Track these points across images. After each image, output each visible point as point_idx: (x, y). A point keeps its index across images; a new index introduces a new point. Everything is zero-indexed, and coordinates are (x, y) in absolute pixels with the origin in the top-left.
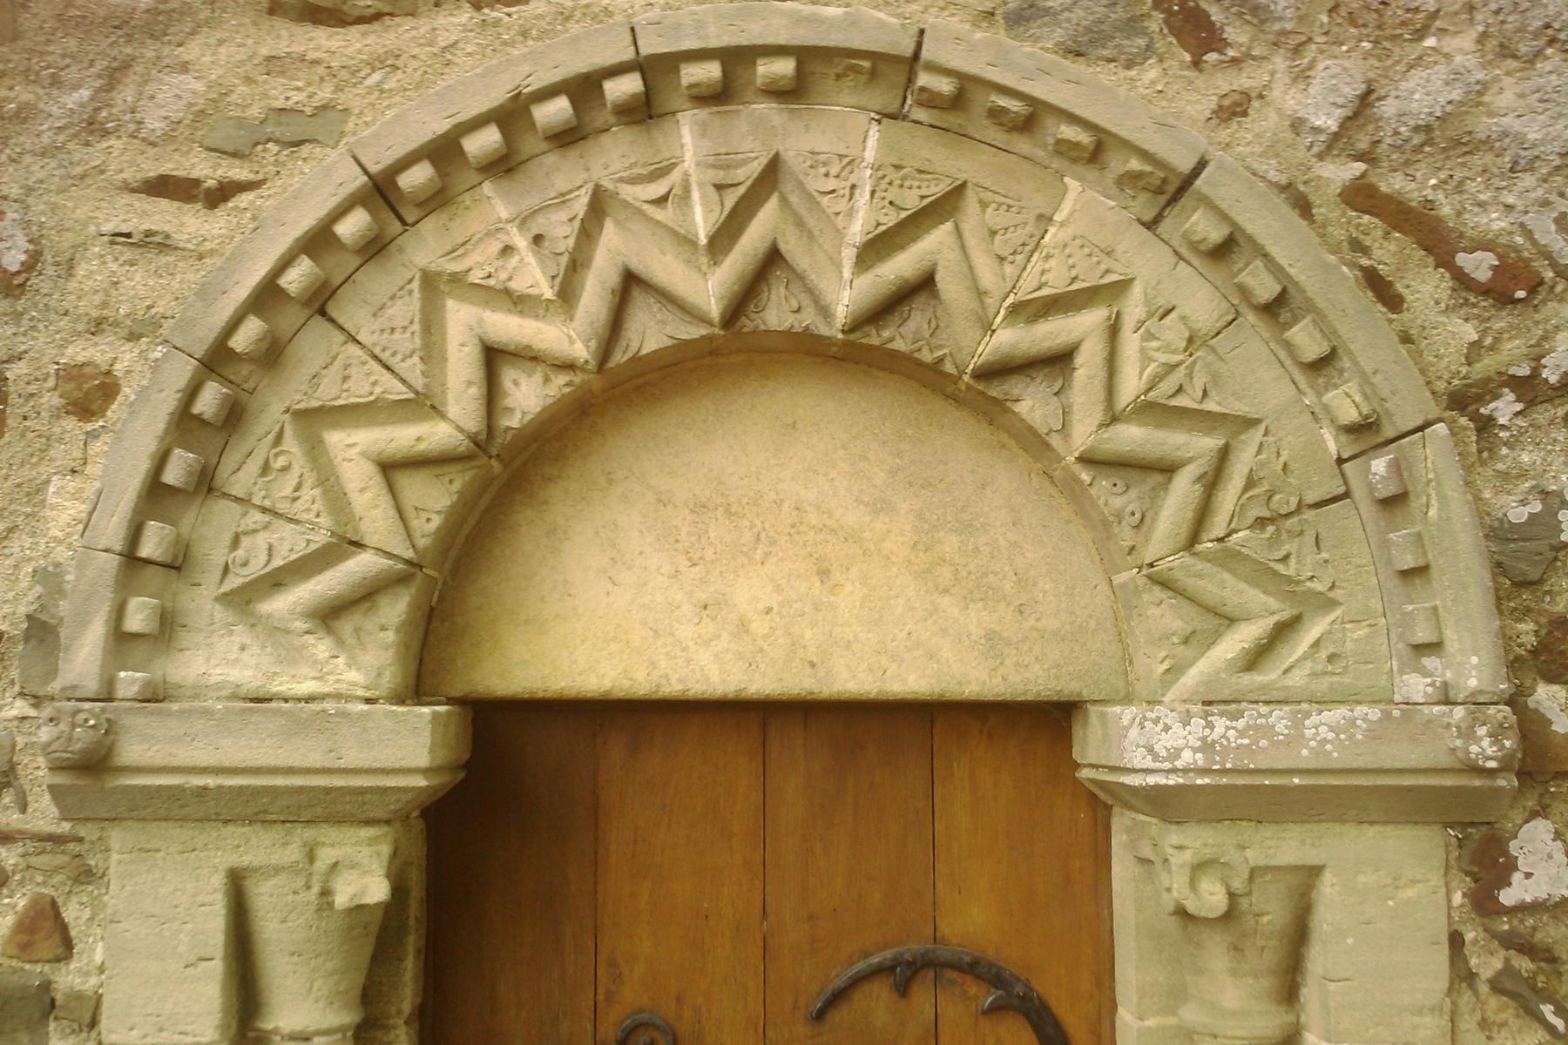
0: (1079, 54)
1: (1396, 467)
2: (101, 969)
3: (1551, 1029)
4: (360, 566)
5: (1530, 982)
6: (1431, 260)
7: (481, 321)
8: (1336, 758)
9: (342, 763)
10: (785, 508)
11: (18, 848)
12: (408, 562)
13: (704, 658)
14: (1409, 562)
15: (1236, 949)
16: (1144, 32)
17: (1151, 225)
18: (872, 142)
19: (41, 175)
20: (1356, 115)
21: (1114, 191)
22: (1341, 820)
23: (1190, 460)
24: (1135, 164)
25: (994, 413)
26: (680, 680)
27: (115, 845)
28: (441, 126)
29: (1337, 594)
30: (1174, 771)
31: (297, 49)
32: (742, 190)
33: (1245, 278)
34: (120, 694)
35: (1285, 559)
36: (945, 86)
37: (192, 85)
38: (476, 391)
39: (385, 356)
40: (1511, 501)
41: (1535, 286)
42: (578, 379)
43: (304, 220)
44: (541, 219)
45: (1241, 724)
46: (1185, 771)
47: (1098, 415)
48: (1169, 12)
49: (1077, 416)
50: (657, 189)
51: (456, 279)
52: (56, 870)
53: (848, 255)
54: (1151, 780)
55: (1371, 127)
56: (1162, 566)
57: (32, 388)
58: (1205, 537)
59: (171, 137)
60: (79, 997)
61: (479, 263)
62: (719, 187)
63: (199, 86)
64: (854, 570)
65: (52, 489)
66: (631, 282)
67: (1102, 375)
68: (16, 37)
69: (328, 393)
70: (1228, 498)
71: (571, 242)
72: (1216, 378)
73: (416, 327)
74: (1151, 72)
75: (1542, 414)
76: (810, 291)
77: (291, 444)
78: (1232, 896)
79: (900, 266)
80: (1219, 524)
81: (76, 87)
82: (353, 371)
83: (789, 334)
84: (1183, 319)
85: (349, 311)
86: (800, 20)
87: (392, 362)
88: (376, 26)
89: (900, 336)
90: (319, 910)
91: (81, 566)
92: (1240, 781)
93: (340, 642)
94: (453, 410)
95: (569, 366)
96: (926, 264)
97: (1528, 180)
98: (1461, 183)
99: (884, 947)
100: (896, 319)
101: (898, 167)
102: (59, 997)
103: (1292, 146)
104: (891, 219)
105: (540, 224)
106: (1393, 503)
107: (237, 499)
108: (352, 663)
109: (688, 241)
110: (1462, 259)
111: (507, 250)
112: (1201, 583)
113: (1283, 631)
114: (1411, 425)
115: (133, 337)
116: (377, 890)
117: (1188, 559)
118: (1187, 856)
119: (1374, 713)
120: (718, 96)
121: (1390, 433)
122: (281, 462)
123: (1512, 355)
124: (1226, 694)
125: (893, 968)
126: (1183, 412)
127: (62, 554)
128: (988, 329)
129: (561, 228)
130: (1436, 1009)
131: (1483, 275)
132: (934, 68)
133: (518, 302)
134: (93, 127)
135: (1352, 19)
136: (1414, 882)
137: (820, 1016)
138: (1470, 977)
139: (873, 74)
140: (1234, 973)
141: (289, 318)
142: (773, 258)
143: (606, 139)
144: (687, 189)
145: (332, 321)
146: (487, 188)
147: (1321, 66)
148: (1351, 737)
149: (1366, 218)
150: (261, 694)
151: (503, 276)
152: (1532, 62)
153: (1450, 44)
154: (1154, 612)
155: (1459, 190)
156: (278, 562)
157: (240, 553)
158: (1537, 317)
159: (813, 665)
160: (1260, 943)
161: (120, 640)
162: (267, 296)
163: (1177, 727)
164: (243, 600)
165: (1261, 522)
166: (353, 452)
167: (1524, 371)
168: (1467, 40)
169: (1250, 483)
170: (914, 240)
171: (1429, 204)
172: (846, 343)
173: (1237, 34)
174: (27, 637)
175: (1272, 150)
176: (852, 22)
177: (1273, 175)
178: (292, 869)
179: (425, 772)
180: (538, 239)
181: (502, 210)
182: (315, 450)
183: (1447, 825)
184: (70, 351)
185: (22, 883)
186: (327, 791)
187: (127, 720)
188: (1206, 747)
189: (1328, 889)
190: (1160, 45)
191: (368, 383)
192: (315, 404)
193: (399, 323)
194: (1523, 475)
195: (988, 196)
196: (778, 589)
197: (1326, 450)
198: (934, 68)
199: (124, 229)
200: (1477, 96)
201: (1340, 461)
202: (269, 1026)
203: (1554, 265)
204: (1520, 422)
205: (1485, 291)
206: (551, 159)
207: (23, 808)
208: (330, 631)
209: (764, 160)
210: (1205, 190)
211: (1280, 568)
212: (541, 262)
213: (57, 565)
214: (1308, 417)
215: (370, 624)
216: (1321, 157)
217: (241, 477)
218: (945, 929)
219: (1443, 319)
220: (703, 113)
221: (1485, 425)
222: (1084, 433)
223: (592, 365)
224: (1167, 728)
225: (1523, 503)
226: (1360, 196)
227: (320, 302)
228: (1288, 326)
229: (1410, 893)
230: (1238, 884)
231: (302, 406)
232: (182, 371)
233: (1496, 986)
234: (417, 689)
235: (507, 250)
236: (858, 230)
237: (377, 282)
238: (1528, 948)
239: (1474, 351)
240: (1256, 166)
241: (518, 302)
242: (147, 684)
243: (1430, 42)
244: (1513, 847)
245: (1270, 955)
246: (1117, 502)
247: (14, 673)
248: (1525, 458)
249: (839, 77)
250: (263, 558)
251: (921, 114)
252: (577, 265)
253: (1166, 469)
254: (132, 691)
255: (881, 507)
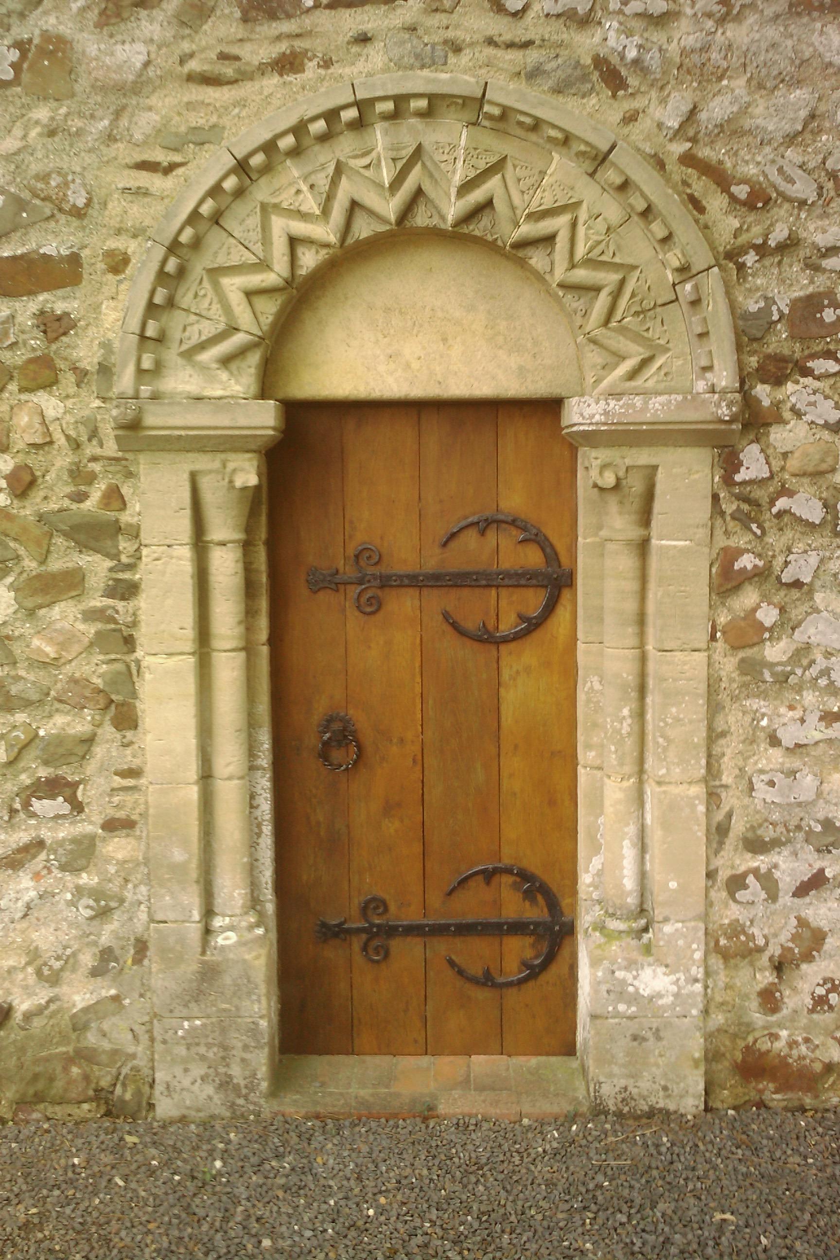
0: (559, 92)
1: (696, 288)
2: (139, 514)
3: (755, 534)
4: (239, 339)
5: (748, 515)
6: (719, 190)
7: (288, 226)
8: (662, 417)
9: (238, 425)
10: (427, 310)
11: (101, 463)
12: (259, 337)
13: (390, 380)
14: (699, 330)
15: (621, 503)
16: (590, 81)
17: (592, 175)
18: (464, 137)
19: (89, 161)
20: (688, 119)
21: (575, 158)
22: (666, 445)
23: (606, 285)
24: (583, 148)
25: (522, 263)
26: (380, 391)
27: (142, 461)
28: (267, 136)
29: (670, 345)
30: (591, 424)
31: (200, 98)
32: (404, 161)
33: (632, 200)
34: (142, 395)
35: (648, 329)
36: (496, 111)
37: (155, 117)
38: (286, 259)
39: (246, 243)
40: (752, 302)
41: (767, 201)
42: (331, 252)
43: (209, 182)
44: (313, 177)
45: (621, 403)
46: (597, 424)
47: (566, 265)
48: (601, 71)
49: (556, 265)
50: (365, 161)
51: (276, 206)
52: (118, 472)
53: (453, 191)
54: (582, 428)
55: (695, 125)
56: (593, 334)
57: (93, 261)
58: (613, 320)
59: (144, 144)
60: (131, 525)
61: (286, 199)
62: (394, 160)
63: (157, 118)
64: (458, 339)
65: (104, 306)
66: (354, 205)
67: (568, 246)
68: (73, 95)
69: (222, 260)
70: (623, 303)
71: (327, 187)
72: (619, 247)
73: (259, 229)
74: (593, 100)
75: (767, 262)
76: (436, 207)
77: (206, 284)
78: (618, 479)
79: (477, 196)
80: (618, 315)
81: (101, 119)
82: (232, 250)
83: (427, 228)
84: (605, 219)
85: (229, 222)
86: (428, 81)
87: (249, 246)
88: (235, 86)
89: (476, 229)
90: (229, 489)
91: (122, 340)
92: (620, 428)
93: (231, 373)
94: (277, 267)
95: (327, 245)
96: (489, 195)
97: (767, 149)
98: (737, 151)
99: (474, 514)
100: (476, 220)
101: (476, 149)
102: (123, 526)
103: (657, 135)
104: (472, 174)
105: (313, 179)
106: (695, 303)
107: (184, 310)
108: (237, 382)
109: (381, 186)
110: (734, 189)
111: (298, 192)
112: (609, 342)
113: (645, 363)
114: (702, 268)
115: (135, 236)
116: (253, 480)
117: (603, 330)
118: (599, 461)
119: (680, 398)
120: (394, 116)
121: (694, 271)
122: (202, 293)
123: (755, 235)
124: (618, 391)
125: (478, 523)
126: (604, 263)
127: (111, 335)
128: (517, 225)
129: (323, 181)
130: (704, 526)
131: (743, 196)
132: (491, 103)
133: (304, 216)
134: (110, 138)
135: (689, 72)
136: (697, 472)
137: (445, 545)
138: (722, 513)
139: (464, 105)
140: (620, 513)
141: (203, 226)
142: (419, 193)
143: (341, 138)
144: (379, 161)
145: (221, 227)
146: (288, 162)
147: (672, 96)
148: (669, 408)
149: (690, 170)
150: (200, 396)
151: (297, 204)
152: (773, 91)
153: (735, 83)
154: (590, 355)
155: (736, 154)
156: (204, 338)
157: (187, 334)
158: (769, 215)
159: (440, 383)
160: (631, 499)
161: (140, 372)
162: (194, 217)
163: (593, 405)
164: (189, 355)
165: (637, 314)
166: (233, 288)
167: (760, 241)
168: (742, 81)
169: (633, 295)
170: (484, 182)
171: (721, 162)
172: (453, 232)
173: (633, 81)
174: (98, 372)
175: (648, 138)
176: (453, 81)
177: (648, 150)
178: (217, 472)
179: (274, 429)
180: (312, 187)
181: (296, 173)
182: (217, 286)
183: (713, 448)
184: (108, 243)
185: (103, 478)
186: (231, 436)
187: (146, 407)
188: (606, 413)
189: (660, 476)
190: (597, 87)
191: (239, 256)
192: (216, 266)
193: (251, 227)
194: (758, 289)
195: (517, 162)
196: (424, 348)
197: (667, 279)
198: (491, 103)
199: (128, 186)
200: (745, 110)
201: (674, 285)
202: (208, 538)
203: (776, 190)
204: (757, 265)
205: (744, 204)
206: (317, 148)
207: (101, 446)
208: (227, 368)
209: (414, 147)
210: (614, 160)
211: (645, 334)
212: (314, 197)
213: (109, 340)
214: (660, 264)
215: (244, 365)
216: (671, 140)
217: (186, 299)
218: (503, 505)
219: (724, 217)
220: (386, 124)
221: (741, 267)
222: (559, 274)
223: (338, 245)
224: (589, 405)
225: (756, 302)
226: (688, 159)
227: (216, 219)
228: (650, 223)
229: (696, 476)
230: (621, 474)
231: (210, 267)
232: (159, 252)
233: (733, 518)
234: (263, 394)
235: (298, 192)
236: (457, 179)
237: (241, 209)
238: (747, 500)
239: (736, 234)
240: (640, 146)
241: (304, 216)
242: (153, 392)
243: (725, 82)
244: (741, 456)
245: (636, 504)
246: (575, 305)
247: (94, 388)
248: (759, 282)
249: (448, 106)
250: (197, 336)
251: (486, 123)
252: (330, 197)
253: (597, 289)
254: (147, 395)
255: (471, 308)
